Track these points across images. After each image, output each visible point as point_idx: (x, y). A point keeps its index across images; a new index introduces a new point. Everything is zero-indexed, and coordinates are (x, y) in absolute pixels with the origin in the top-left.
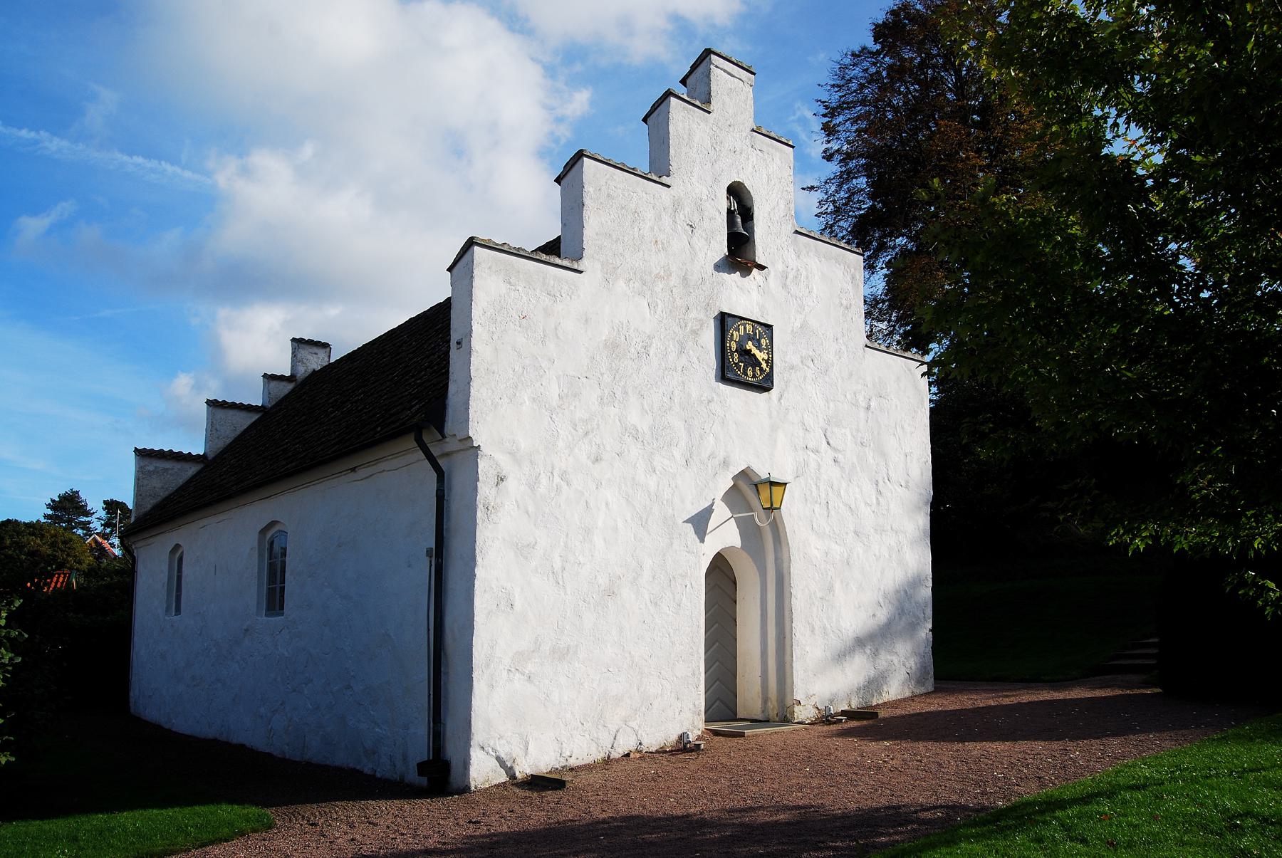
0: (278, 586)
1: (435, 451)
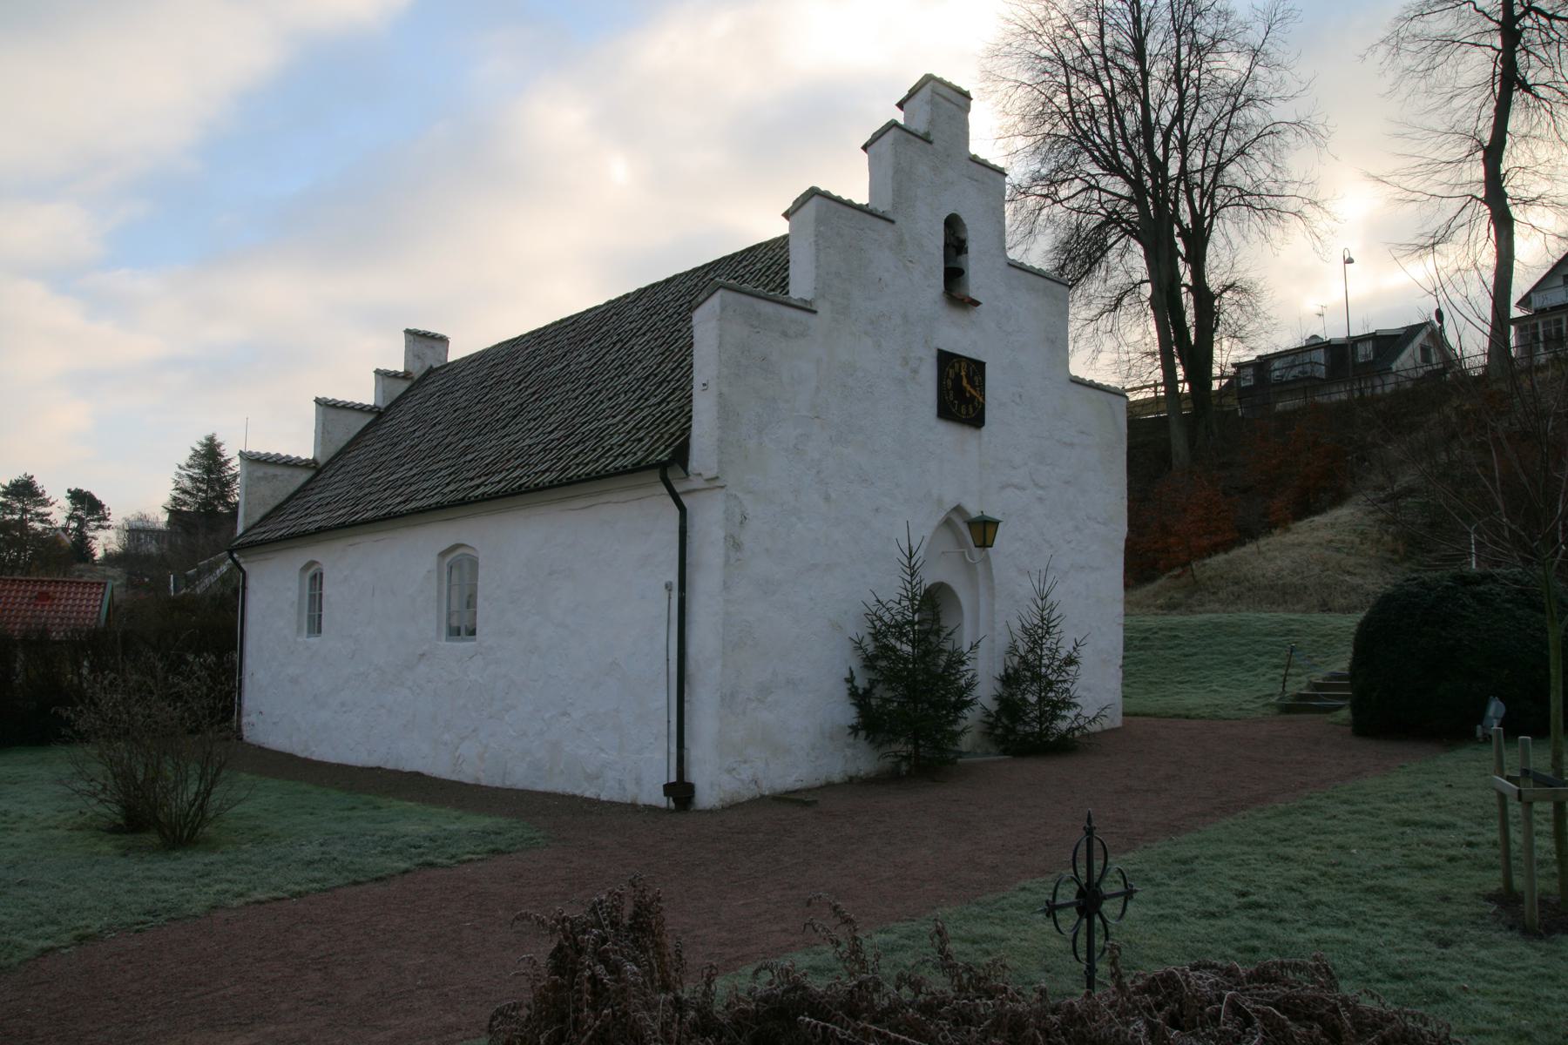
0: (318, 592)
1: (678, 488)
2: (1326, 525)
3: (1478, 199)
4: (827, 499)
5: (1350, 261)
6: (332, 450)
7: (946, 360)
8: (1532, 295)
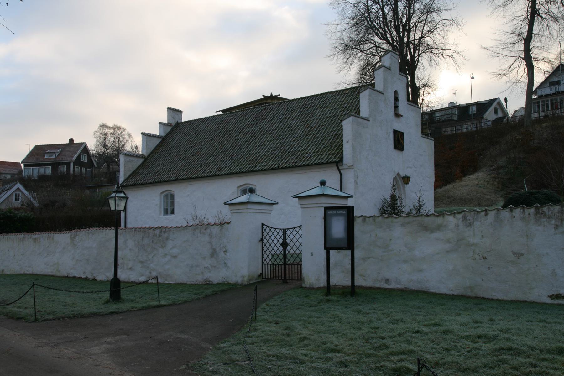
1: (340, 168)
2: (475, 179)
3: (521, 58)
4: (373, 171)
5: (473, 78)
6: (149, 152)
7: (395, 132)
8: (538, 90)
